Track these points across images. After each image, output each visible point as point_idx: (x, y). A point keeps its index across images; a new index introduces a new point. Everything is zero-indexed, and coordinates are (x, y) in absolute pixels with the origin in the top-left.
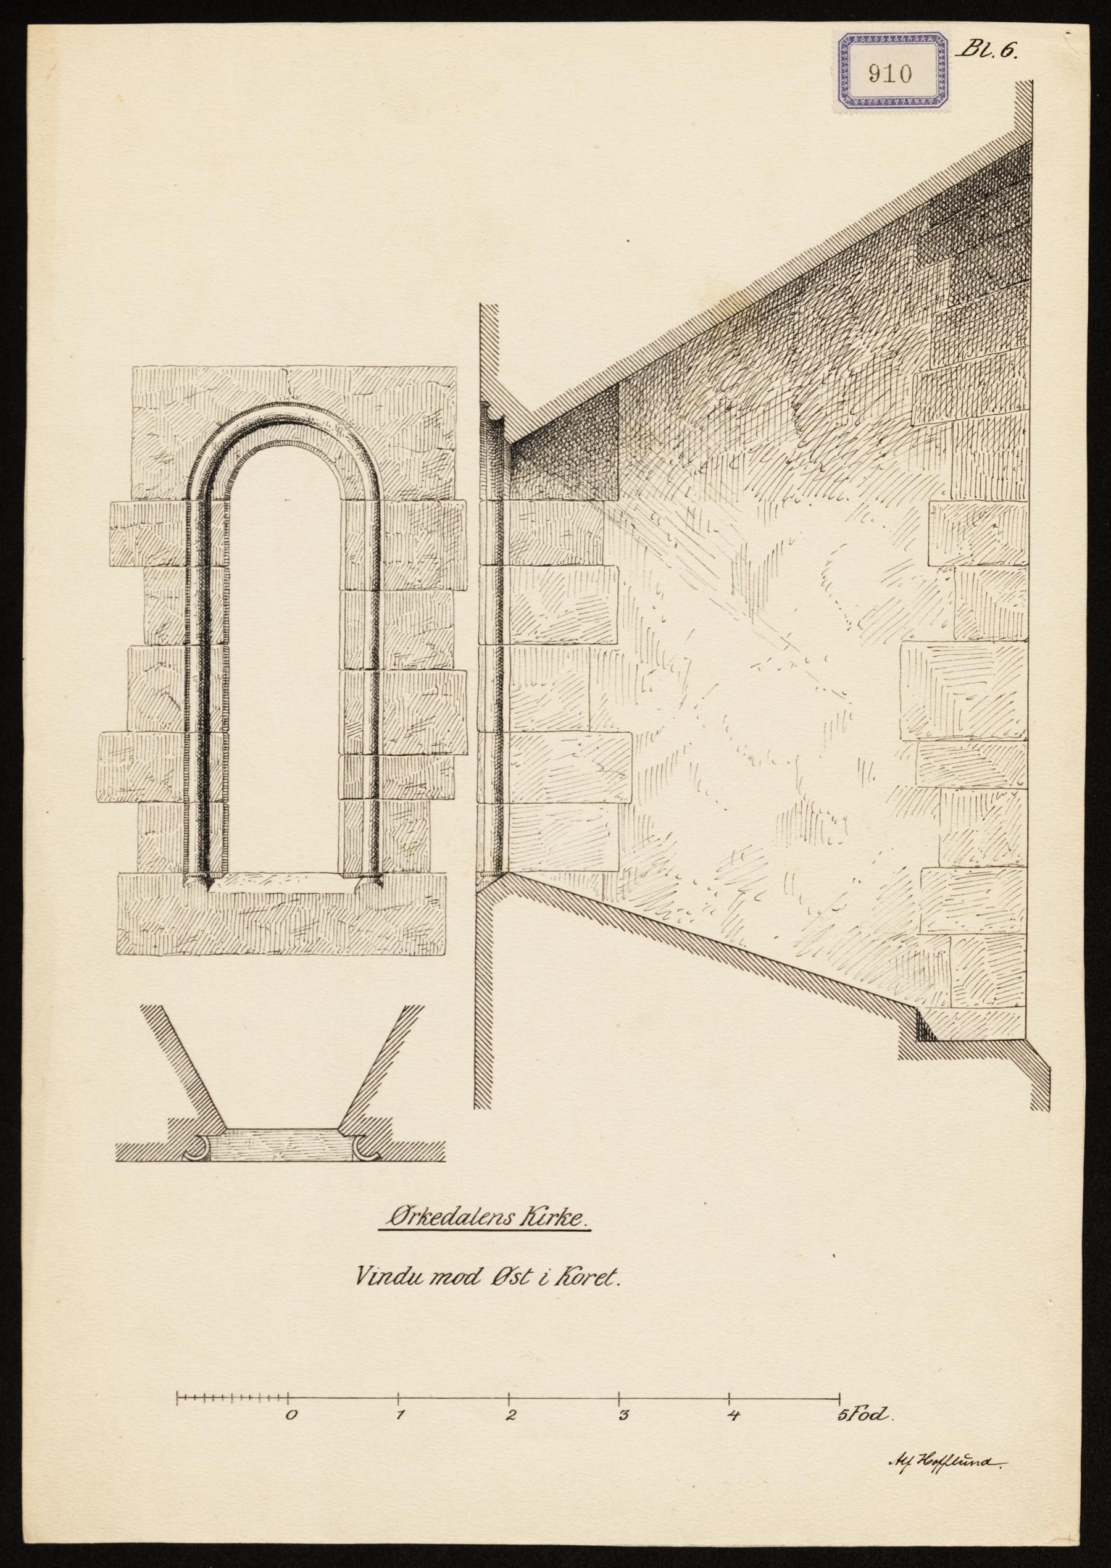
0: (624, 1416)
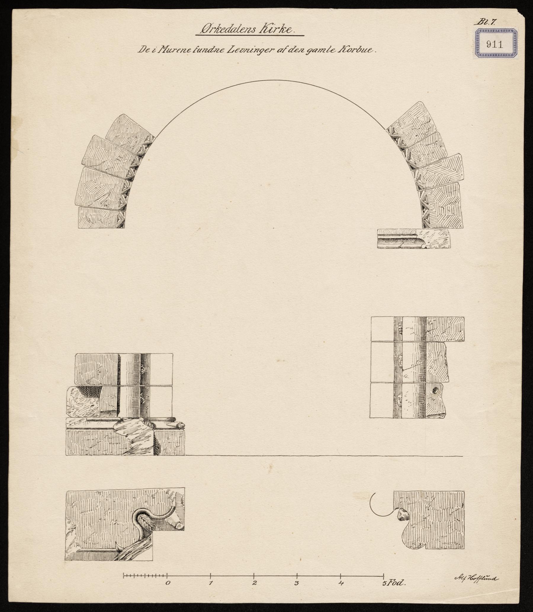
0: (296, 584)
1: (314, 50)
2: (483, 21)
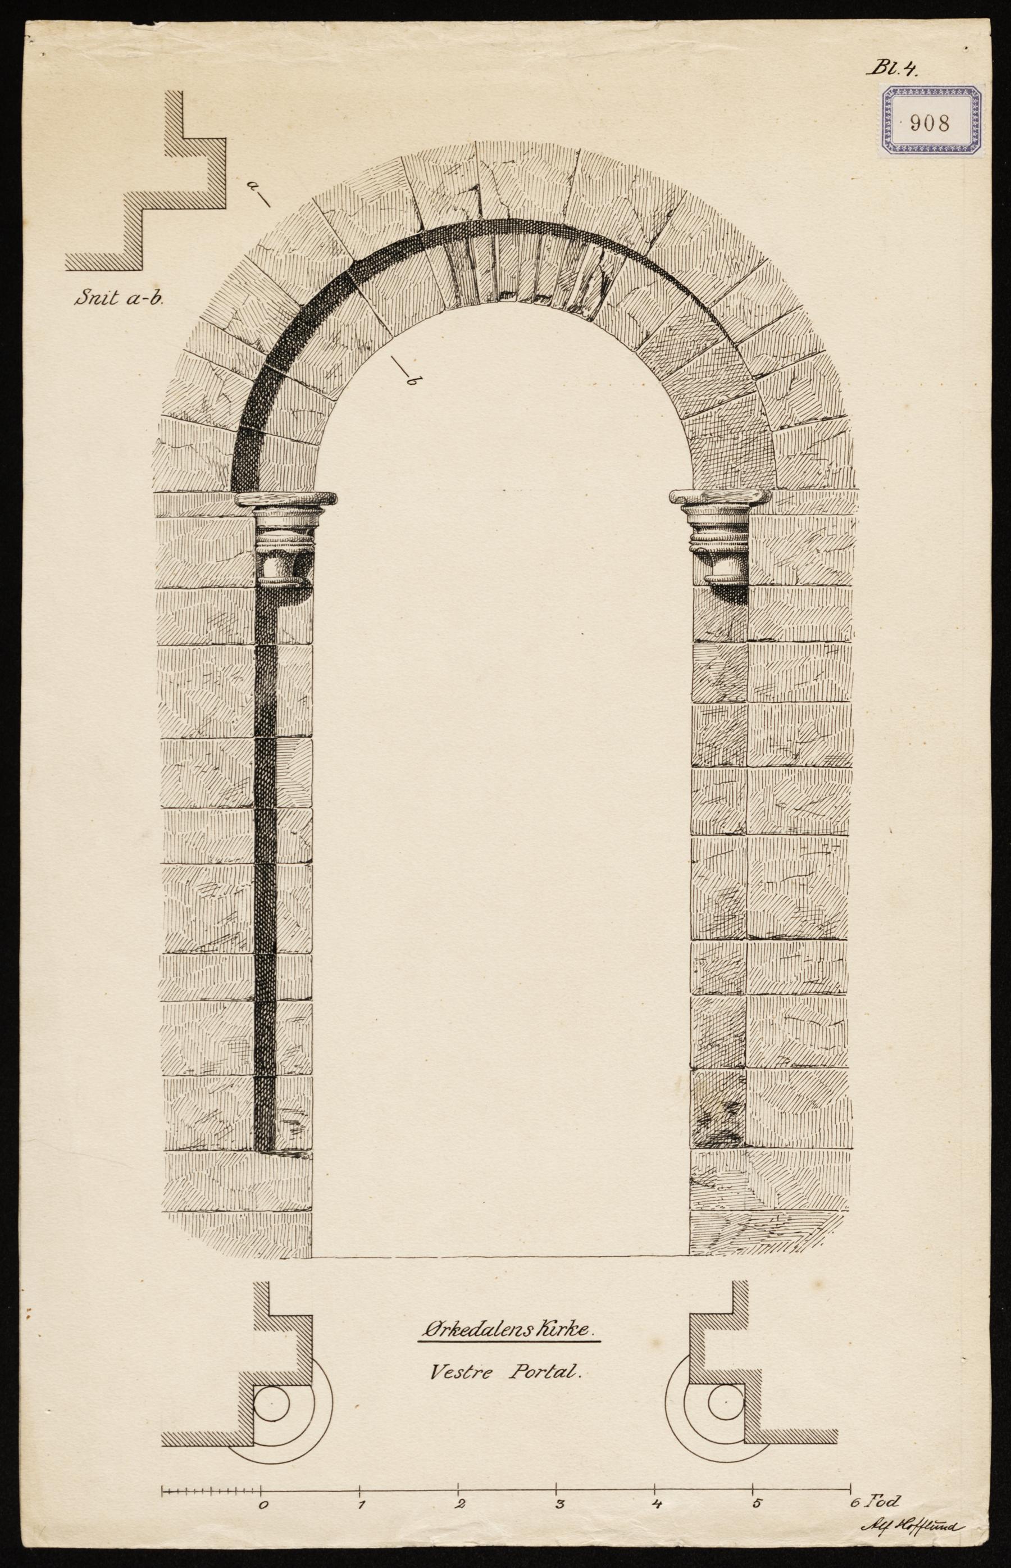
1: (472, 1330)
2: (885, 66)
